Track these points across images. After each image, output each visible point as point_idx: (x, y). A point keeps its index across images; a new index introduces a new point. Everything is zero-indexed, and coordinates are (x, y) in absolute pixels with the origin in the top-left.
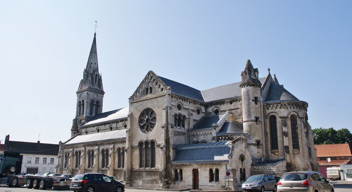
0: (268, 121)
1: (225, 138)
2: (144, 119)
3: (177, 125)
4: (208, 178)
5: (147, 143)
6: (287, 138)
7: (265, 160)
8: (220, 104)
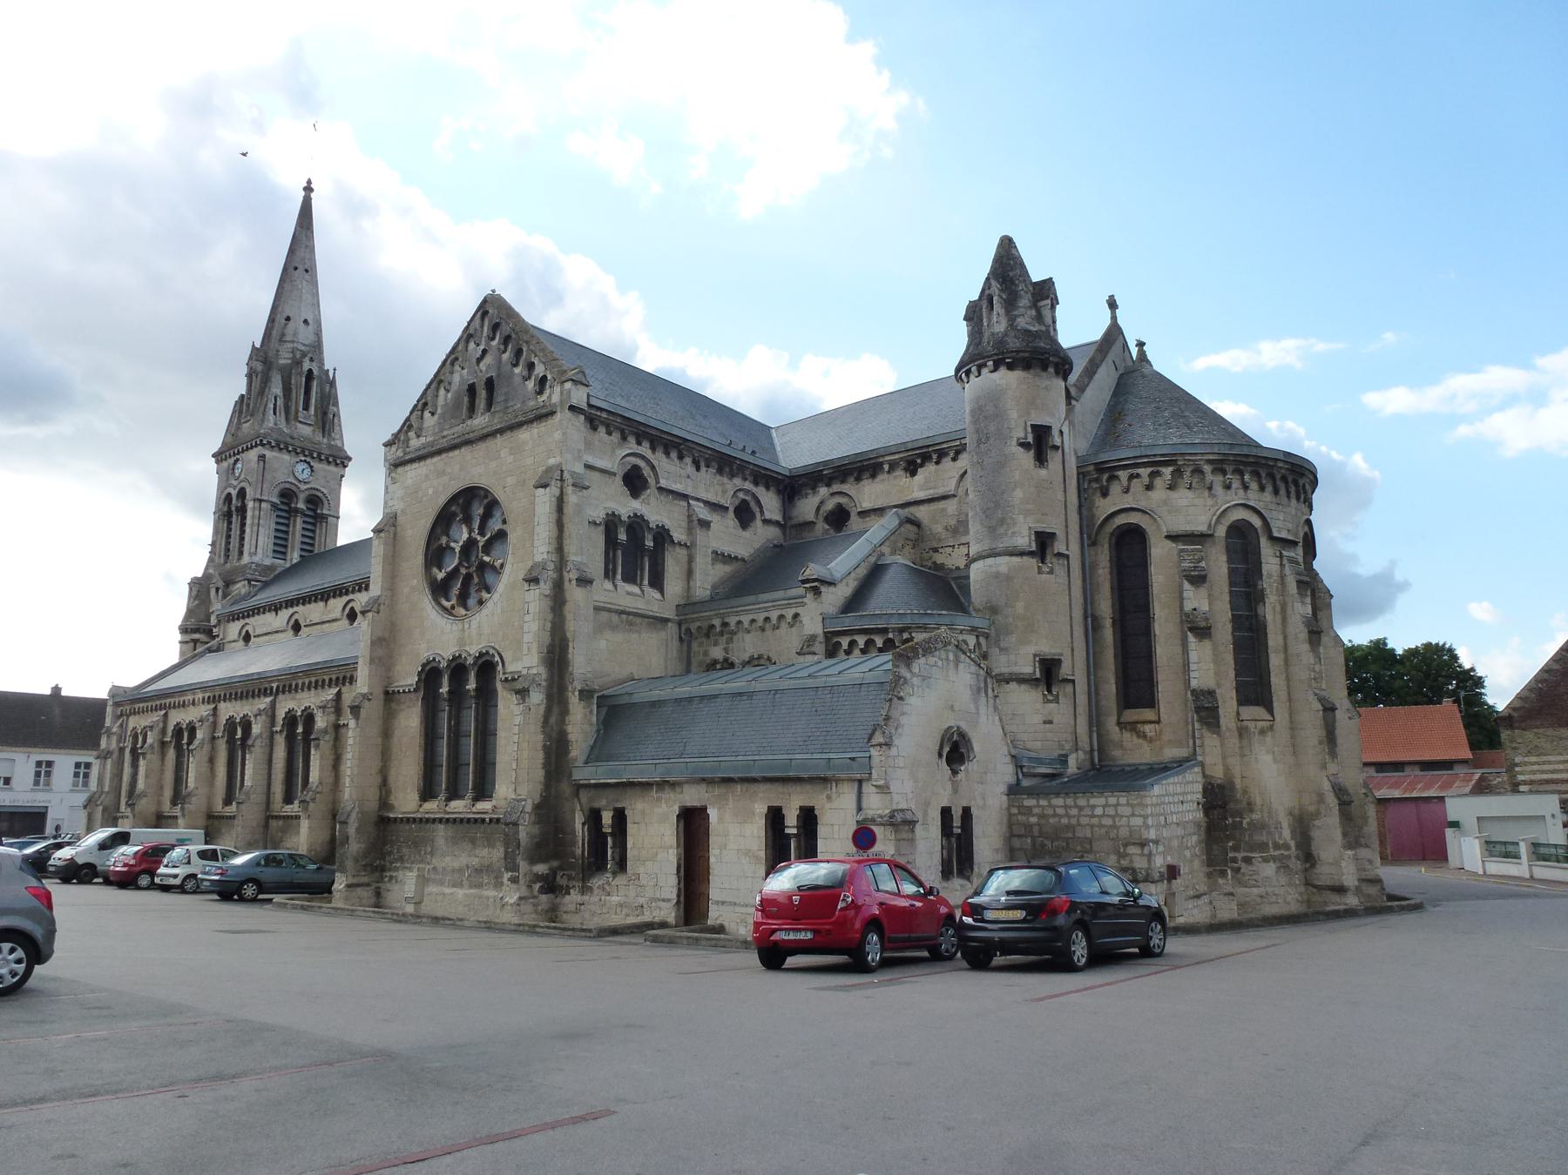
0: (1103, 556)
1: (870, 643)
3: (619, 577)
4: (757, 858)
5: (458, 669)
6: (1207, 644)
7: (1088, 765)
8: (858, 479)
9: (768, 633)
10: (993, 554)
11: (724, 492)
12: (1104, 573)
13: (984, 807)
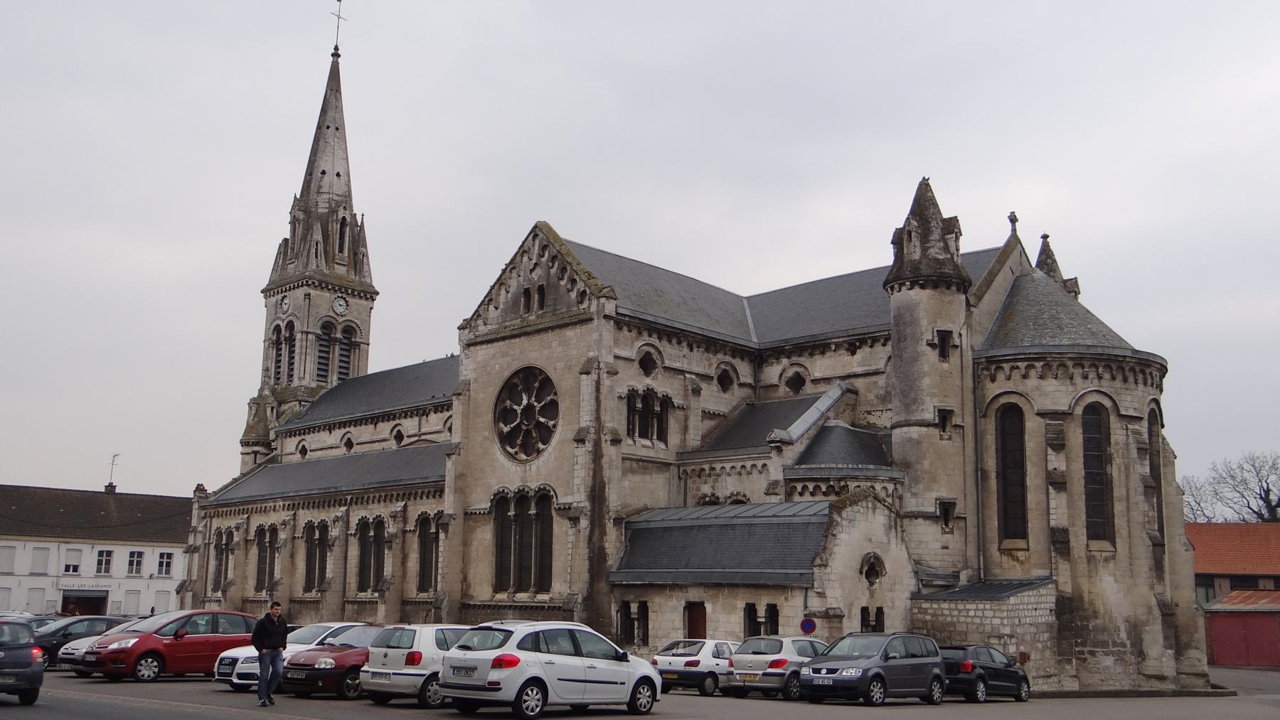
0: (990, 426)
1: (817, 488)
2: (515, 407)
5: (522, 497)
6: (1063, 496)
8: (812, 355)
9: (744, 476)
10: (908, 424)
11: (710, 365)
12: (990, 440)
13: (893, 607)
